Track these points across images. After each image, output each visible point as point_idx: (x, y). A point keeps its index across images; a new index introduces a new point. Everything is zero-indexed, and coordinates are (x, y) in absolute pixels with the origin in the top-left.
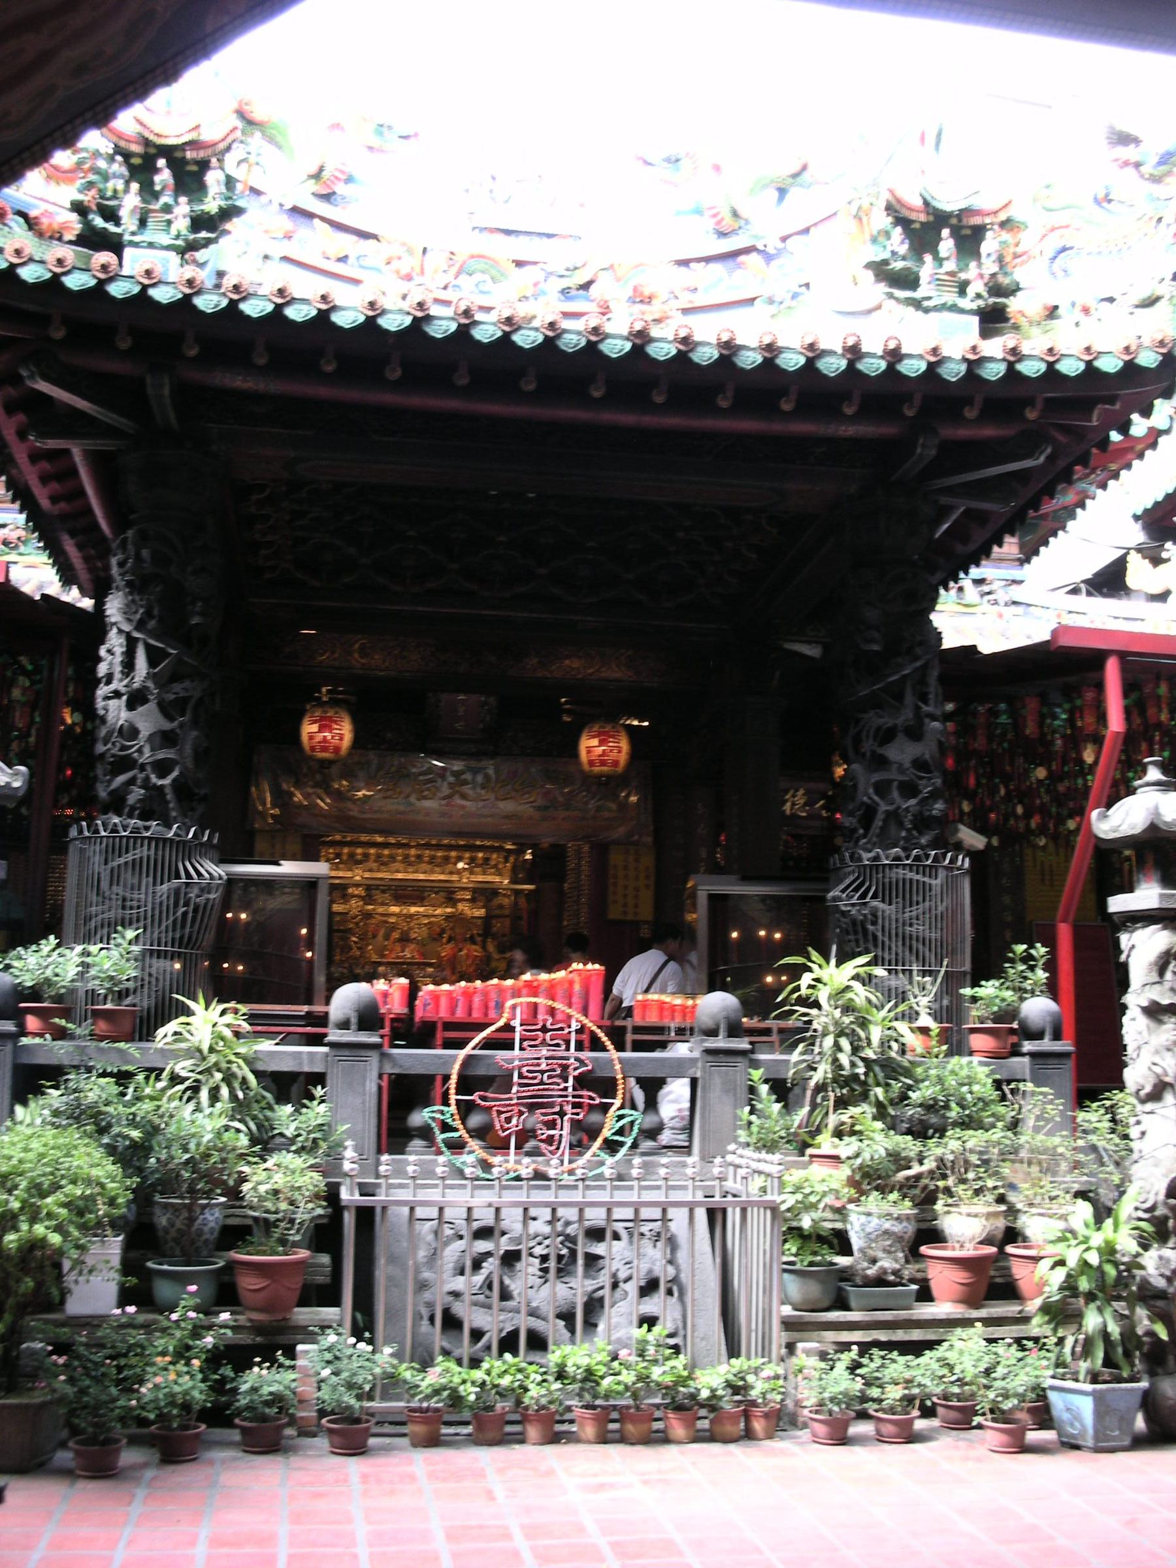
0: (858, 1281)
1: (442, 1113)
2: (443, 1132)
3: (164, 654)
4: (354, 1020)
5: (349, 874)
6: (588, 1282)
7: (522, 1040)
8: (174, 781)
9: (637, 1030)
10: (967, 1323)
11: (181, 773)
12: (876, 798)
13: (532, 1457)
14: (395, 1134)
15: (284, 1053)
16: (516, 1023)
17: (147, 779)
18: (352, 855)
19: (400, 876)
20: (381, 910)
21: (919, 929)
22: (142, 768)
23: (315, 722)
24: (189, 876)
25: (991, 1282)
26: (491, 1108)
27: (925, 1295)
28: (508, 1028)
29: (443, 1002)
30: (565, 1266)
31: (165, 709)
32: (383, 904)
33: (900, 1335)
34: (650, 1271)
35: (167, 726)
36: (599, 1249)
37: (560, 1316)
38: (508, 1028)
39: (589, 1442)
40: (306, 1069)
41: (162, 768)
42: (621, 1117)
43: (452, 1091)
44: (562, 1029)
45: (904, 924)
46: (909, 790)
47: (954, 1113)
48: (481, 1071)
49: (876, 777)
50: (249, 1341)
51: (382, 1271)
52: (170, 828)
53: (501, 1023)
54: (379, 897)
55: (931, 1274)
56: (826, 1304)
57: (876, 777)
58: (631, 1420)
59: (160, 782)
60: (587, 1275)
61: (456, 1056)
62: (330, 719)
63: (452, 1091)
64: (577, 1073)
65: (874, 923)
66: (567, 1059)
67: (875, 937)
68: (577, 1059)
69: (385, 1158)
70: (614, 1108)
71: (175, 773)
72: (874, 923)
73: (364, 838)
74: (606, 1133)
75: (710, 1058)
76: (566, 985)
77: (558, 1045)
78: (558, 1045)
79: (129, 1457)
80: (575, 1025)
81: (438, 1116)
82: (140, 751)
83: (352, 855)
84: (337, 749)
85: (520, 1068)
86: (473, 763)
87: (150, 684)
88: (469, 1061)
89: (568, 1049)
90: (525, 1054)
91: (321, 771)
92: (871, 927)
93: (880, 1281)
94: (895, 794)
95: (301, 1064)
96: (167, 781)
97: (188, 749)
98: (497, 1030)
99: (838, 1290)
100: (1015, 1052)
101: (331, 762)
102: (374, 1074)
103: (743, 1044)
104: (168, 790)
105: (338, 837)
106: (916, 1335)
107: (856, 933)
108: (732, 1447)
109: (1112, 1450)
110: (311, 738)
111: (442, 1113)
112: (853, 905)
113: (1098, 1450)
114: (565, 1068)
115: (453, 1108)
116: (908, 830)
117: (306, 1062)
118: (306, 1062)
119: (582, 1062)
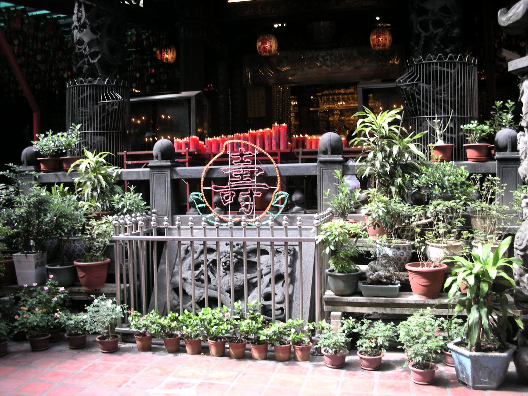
0: (369, 281)
1: (198, 195)
2: (198, 204)
3: (92, 6)
4: (159, 156)
5: (333, 106)
6: (248, 275)
7: (231, 161)
8: (99, 60)
9: (304, 153)
10: (424, 306)
11: (102, 57)
12: (420, 30)
13: (188, 359)
14: (180, 206)
15: (133, 172)
16: (229, 152)
17: (89, 60)
18: (333, 99)
19: (352, 105)
20: (347, 119)
21: (444, 96)
22: (87, 56)
23: (260, 41)
24: (113, 98)
25: (436, 283)
26: (219, 192)
27: (406, 287)
28: (226, 155)
29: (214, 146)
30: (238, 267)
31: (93, 30)
32: (348, 116)
33: (388, 311)
34: (278, 270)
35: (95, 37)
36: (254, 259)
37: (226, 291)
38: (226, 155)
39: (213, 356)
40: (142, 178)
41: (93, 55)
42: (278, 196)
43: (202, 185)
44: (250, 154)
45: (437, 94)
46: (438, 24)
47: (437, 191)
48: (215, 176)
49: (420, 19)
50: (85, 299)
51: (303, 261)
52: (96, 79)
53: (221, 153)
54: (346, 114)
55: (410, 278)
56: (348, 292)
57: (420, 19)
58: (235, 346)
59: (93, 62)
60: (248, 272)
61: (203, 170)
62: (266, 40)
63: (202, 185)
64: (257, 175)
65: (419, 94)
66: (254, 168)
67: (419, 101)
68: (258, 168)
69: (178, 217)
70: (276, 191)
71: (100, 56)
72: (419, 94)
73: (337, 91)
74: (272, 203)
75: (322, 165)
76: (269, 134)
77: (249, 162)
78: (249, 162)
79: (13, 347)
80: (256, 152)
81: (196, 197)
82: (85, 50)
83: (333, 99)
84: (270, 51)
85: (231, 173)
86: (329, 52)
87: (87, 21)
88: (209, 171)
89: (253, 163)
90: (233, 167)
91: (267, 60)
92: (417, 96)
93: (378, 281)
94: (431, 27)
95: (140, 176)
96: (95, 61)
97: (105, 45)
98: (218, 158)
99: (354, 283)
100: (491, 158)
101: (269, 57)
102: (169, 180)
103: (340, 158)
104: (96, 65)
105: (327, 92)
106: (398, 311)
107: (409, 100)
108: (280, 364)
109: (485, 389)
110: (259, 48)
111: (198, 195)
112: (408, 85)
113: (475, 388)
114: (252, 173)
115: (202, 194)
116: (438, 45)
117: (141, 175)
118: (141, 175)
119: (260, 170)
